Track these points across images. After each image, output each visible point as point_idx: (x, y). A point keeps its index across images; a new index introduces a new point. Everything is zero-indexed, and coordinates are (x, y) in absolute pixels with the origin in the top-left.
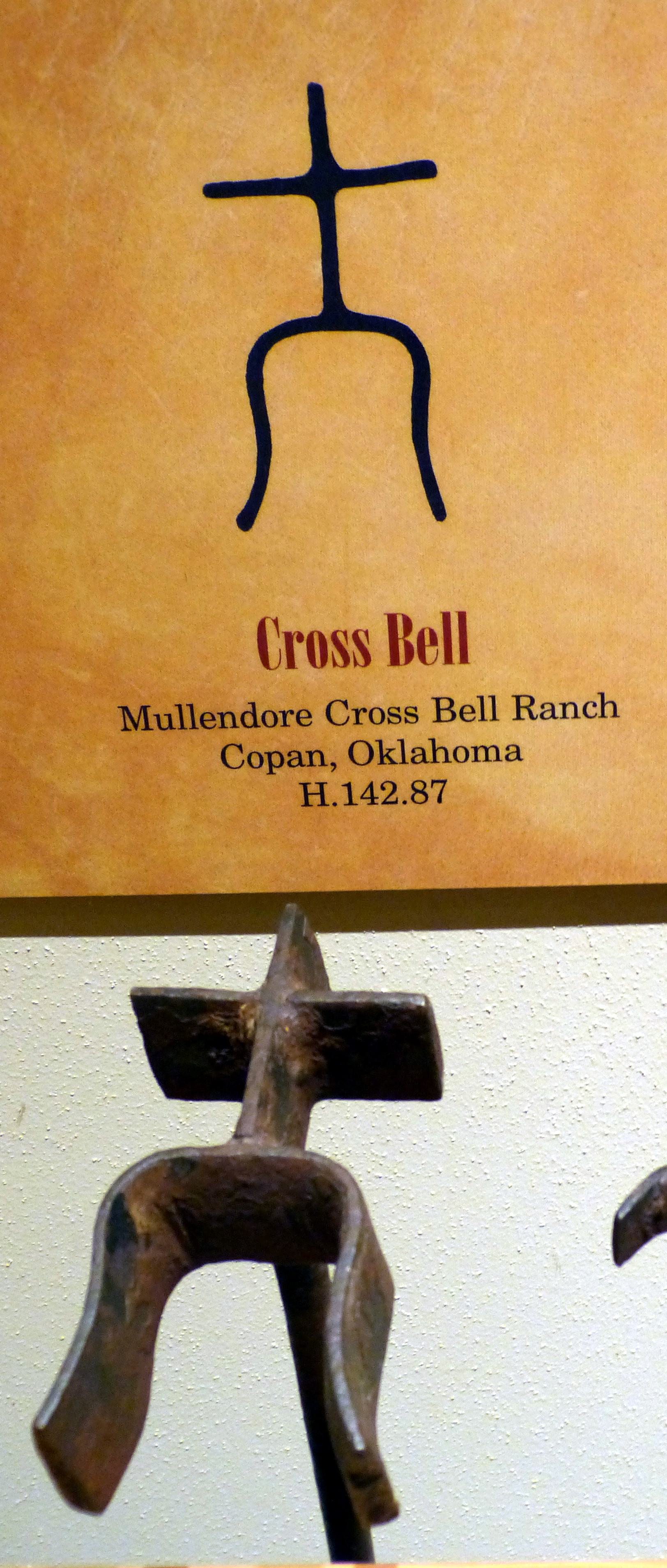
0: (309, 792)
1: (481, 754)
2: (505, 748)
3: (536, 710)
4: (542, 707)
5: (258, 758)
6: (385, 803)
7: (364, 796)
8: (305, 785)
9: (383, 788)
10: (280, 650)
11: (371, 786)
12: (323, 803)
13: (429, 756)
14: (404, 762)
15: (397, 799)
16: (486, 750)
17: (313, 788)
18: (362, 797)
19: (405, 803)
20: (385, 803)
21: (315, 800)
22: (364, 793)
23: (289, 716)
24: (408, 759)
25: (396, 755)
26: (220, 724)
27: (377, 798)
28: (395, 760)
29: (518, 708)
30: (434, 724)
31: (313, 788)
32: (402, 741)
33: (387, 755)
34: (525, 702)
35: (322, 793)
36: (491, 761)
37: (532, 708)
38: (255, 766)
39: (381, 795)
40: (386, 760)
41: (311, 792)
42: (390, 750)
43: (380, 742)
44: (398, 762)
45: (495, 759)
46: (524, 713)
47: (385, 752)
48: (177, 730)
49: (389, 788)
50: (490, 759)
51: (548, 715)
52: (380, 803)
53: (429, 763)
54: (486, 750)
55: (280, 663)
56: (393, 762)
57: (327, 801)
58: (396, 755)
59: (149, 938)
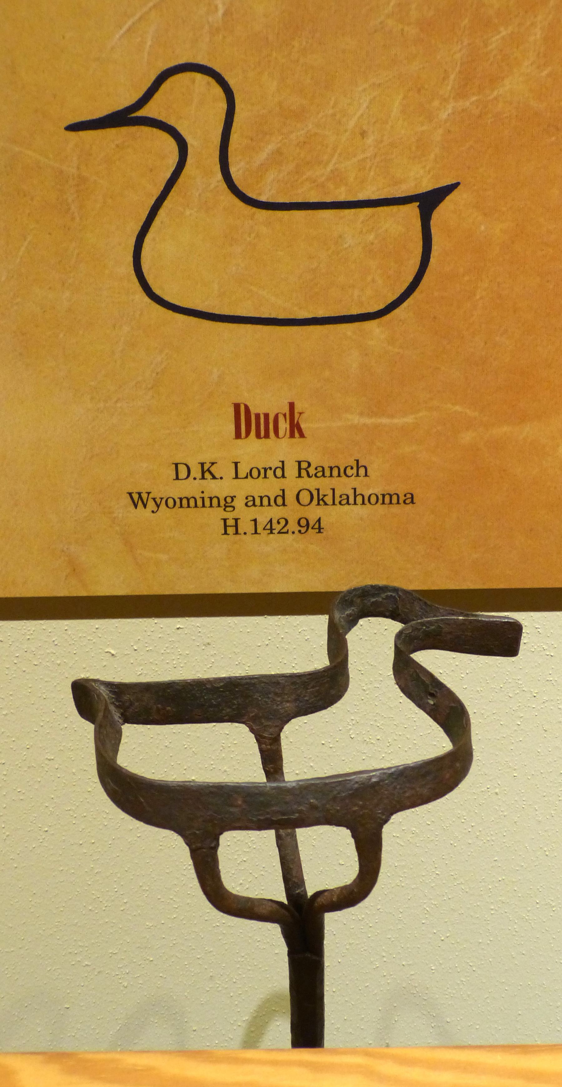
0: (228, 524)
1: (387, 499)
2: (403, 495)
3: (312, 471)
4: (316, 469)
5: (375, 498)
6: (279, 533)
7: (266, 528)
8: (225, 520)
9: (279, 523)
10: (286, 428)
11: (271, 521)
12: (237, 533)
13: (351, 500)
14: (334, 504)
15: (288, 530)
16: (391, 496)
17: (231, 522)
18: (264, 529)
19: (293, 533)
20: (279, 533)
21: (231, 530)
22: (314, 526)
23: (268, 471)
24: (337, 502)
25: (329, 500)
26: (355, 474)
27: (323, 528)
28: (328, 503)
29: (300, 469)
30: (174, 481)
31: (231, 522)
32: (333, 490)
33: (322, 499)
34: (304, 465)
35: (236, 526)
36: (184, 508)
37: (308, 469)
38: (372, 503)
39: (277, 527)
40: (321, 502)
41: (230, 525)
42: (325, 496)
43: (318, 490)
44: (330, 504)
45: (332, 503)
46: (304, 473)
47: (321, 497)
48: (327, 477)
49: (283, 522)
50: (385, 503)
51: (320, 474)
52: (276, 533)
53: (192, 508)
54: (391, 496)
55: (285, 434)
56: (326, 504)
57: (240, 531)
58: (329, 500)
59: (156, 620)
